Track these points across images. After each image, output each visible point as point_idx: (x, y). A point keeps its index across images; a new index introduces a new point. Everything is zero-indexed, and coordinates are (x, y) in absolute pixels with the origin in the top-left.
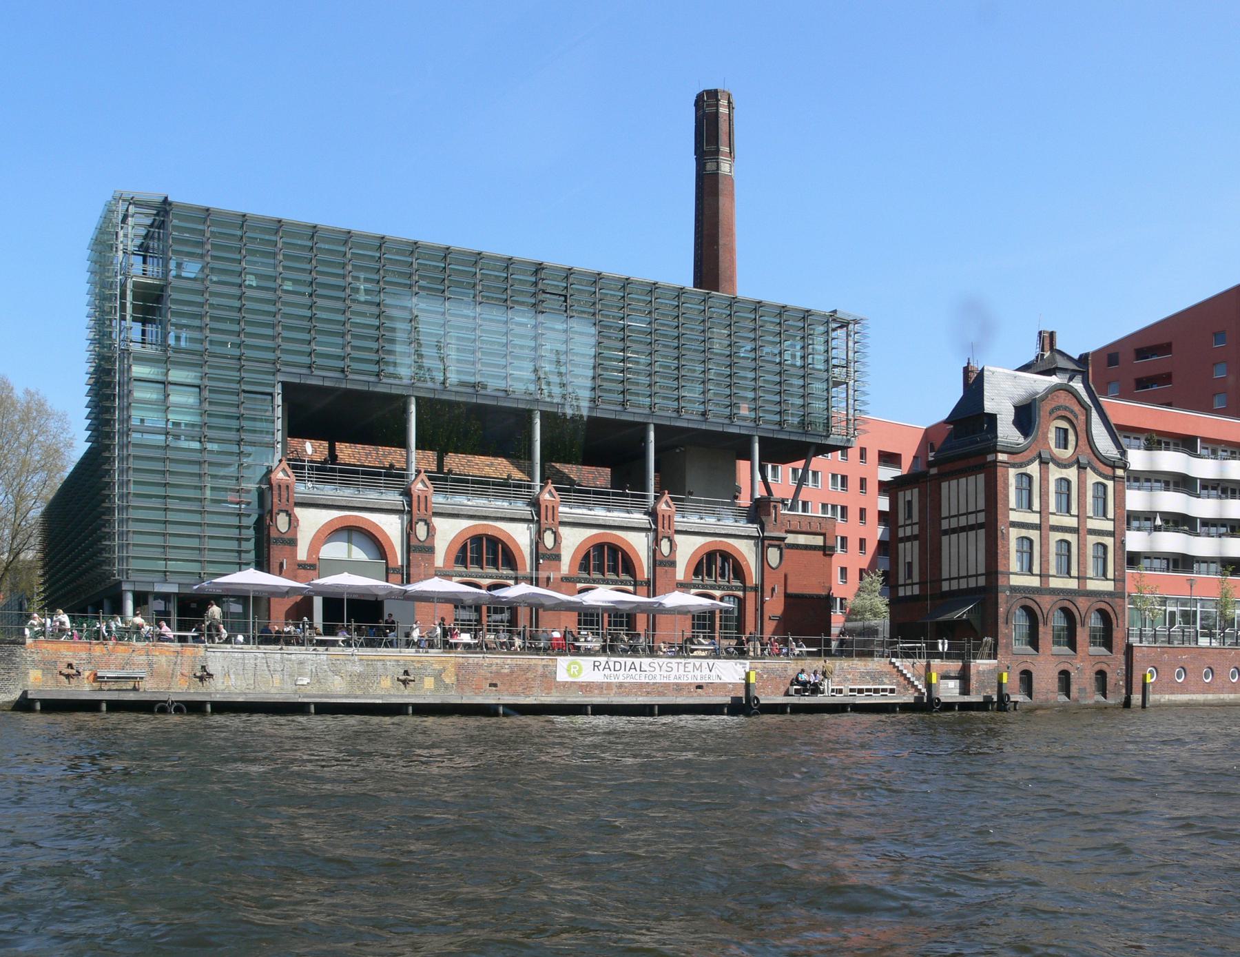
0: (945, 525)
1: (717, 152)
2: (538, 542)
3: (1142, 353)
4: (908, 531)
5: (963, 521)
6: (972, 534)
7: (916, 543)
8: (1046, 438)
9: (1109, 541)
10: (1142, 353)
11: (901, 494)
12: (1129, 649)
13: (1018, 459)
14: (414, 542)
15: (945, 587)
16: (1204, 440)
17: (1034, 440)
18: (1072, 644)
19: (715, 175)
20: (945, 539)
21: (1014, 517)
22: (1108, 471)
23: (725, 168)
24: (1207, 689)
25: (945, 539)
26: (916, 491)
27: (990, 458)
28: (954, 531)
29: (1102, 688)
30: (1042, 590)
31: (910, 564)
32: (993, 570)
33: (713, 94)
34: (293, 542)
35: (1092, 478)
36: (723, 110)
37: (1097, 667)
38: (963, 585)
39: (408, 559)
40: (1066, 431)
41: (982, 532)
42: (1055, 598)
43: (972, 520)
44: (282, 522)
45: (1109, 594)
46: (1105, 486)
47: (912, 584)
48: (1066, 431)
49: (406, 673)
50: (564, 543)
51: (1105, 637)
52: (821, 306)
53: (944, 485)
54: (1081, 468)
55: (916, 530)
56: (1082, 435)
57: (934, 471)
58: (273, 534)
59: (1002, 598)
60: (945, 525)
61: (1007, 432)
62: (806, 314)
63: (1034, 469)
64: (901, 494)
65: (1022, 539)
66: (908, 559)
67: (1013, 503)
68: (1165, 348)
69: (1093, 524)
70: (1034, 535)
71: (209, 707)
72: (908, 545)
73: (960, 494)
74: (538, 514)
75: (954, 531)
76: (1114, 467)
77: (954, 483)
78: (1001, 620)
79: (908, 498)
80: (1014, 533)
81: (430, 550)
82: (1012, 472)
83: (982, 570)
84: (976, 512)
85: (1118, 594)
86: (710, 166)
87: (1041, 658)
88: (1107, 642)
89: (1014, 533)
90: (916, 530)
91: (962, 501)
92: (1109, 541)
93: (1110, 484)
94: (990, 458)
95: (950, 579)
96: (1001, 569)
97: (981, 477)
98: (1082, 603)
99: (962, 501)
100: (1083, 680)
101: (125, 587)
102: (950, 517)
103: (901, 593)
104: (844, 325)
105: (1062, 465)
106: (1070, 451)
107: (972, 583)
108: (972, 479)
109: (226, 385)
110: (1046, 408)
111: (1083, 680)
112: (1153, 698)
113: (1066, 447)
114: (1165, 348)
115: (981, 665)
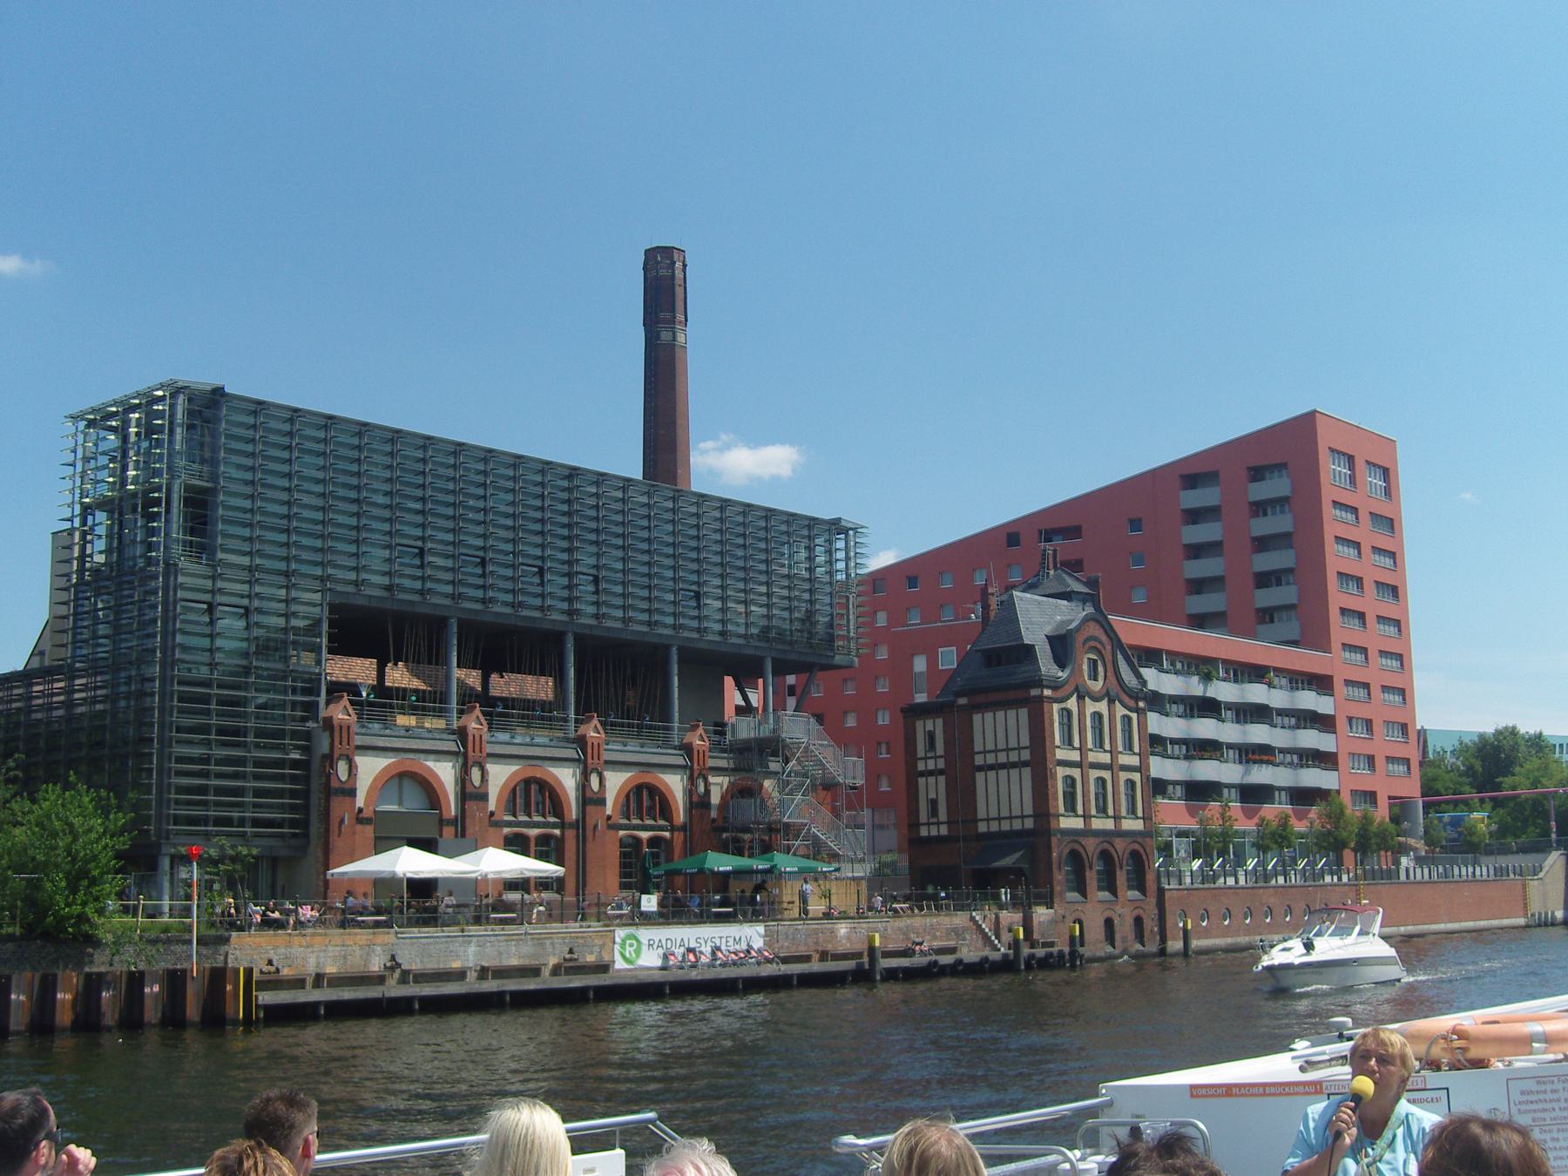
0: (979, 760)
1: (673, 321)
2: (583, 786)
3: (1049, 535)
4: (931, 765)
5: (1002, 758)
6: (1014, 773)
7: (942, 779)
8: (1080, 666)
9: (1136, 777)
10: (1049, 535)
11: (919, 724)
12: (1161, 892)
13: (1060, 694)
14: (469, 789)
15: (982, 827)
16: (1169, 653)
17: (1072, 672)
18: (1113, 890)
19: (671, 347)
20: (980, 777)
21: (1061, 754)
22: (1132, 703)
23: (681, 338)
24: (1226, 932)
25: (980, 777)
26: (939, 722)
27: (1034, 692)
28: (991, 767)
29: (1140, 936)
30: (1087, 832)
31: (934, 804)
32: (1043, 812)
33: (667, 252)
34: (352, 793)
35: (1120, 711)
36: (679, 274)
37: (1136, 912)
38: (1005, 826)
39: (463, 811)
40: (1095, 662)
41: (1027, 772)
42: (1097, 840)
43: (1014, 757)
44: (342, 769)
45: (1139, 833)
46: (1130, 719)
47: (938, 824)
48: (1095, 662)
49: (571, 951)
50: (608, 784)
51: (1139, 883)
52: (826, 514)
53: (977, 718)
54: (1111, 702)
55: (941, 764)
56: (1110, 666)
57: (962, 701)
58: (334, 784)
59: (1054, 841)
60: (979, 760)
61: (1046, 665)
62: (812, 522)
63: (1072, 703)
64: (919, 724)
65: (1066, 778)
66: (932, 795)
67: (1057, 742)
68: (1073, 532)
69: (1093, 757)
70: (1076, 773)
71: (591, 995)
72: (931, 780)
73: (997, 730)
74: (585, 754)
75: (991, 767)
76: (1137, 699)
77: (989, 716)
78: (1055, 866)
79: (930, 727)
80: (1061, 772)
81: (484, 797)
82: (1056, 706)
83: (1029, 810)
84: (1019, 749)
85: (1148, 833)
86: (665, 336)
87: (1088, 906)
88: (1141, 886)
89: (1061, 772)
90: (941, 764)
91: (1001, 736)
92: (1136, 777)
93: (1134, 716)
94: (1034, 692)
95: (988, 820)
96: (1052, 811)
97: (1024, 713)
98: (1119, 844)
99: (1001, 736)
100: (1124, 929)
101: (165, 850)
102: (985, 752)
103: (924, 832)
104: (845, 531)
105: (1096, 699)
106: (1101, 683)
107: (1017, 825)
108: (1011, 713)
109: (1123, 797)
110: (1080, 638)
111: (1124, 929)
112: (1196, 943)
113: (1096, 679)
114: (1073, 532)
115: (1041, 913)
